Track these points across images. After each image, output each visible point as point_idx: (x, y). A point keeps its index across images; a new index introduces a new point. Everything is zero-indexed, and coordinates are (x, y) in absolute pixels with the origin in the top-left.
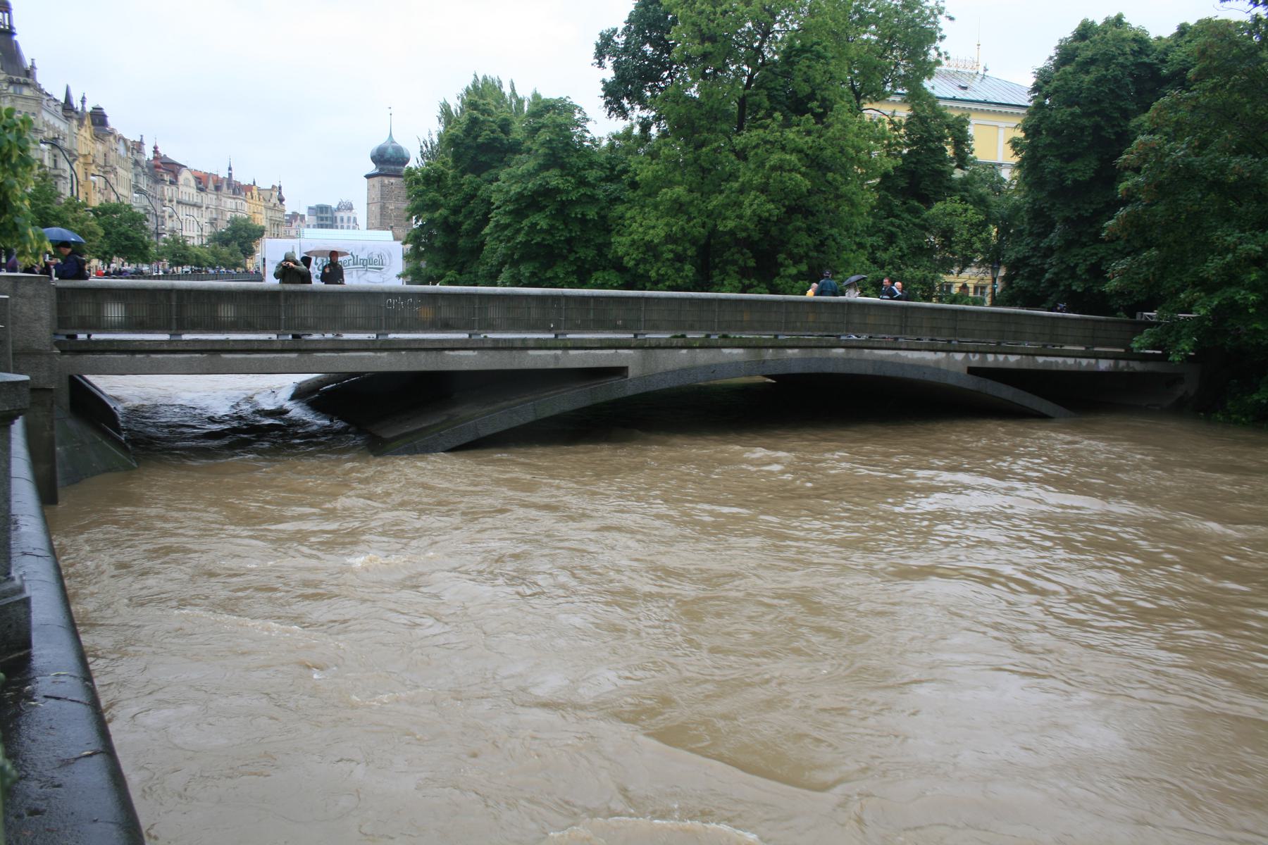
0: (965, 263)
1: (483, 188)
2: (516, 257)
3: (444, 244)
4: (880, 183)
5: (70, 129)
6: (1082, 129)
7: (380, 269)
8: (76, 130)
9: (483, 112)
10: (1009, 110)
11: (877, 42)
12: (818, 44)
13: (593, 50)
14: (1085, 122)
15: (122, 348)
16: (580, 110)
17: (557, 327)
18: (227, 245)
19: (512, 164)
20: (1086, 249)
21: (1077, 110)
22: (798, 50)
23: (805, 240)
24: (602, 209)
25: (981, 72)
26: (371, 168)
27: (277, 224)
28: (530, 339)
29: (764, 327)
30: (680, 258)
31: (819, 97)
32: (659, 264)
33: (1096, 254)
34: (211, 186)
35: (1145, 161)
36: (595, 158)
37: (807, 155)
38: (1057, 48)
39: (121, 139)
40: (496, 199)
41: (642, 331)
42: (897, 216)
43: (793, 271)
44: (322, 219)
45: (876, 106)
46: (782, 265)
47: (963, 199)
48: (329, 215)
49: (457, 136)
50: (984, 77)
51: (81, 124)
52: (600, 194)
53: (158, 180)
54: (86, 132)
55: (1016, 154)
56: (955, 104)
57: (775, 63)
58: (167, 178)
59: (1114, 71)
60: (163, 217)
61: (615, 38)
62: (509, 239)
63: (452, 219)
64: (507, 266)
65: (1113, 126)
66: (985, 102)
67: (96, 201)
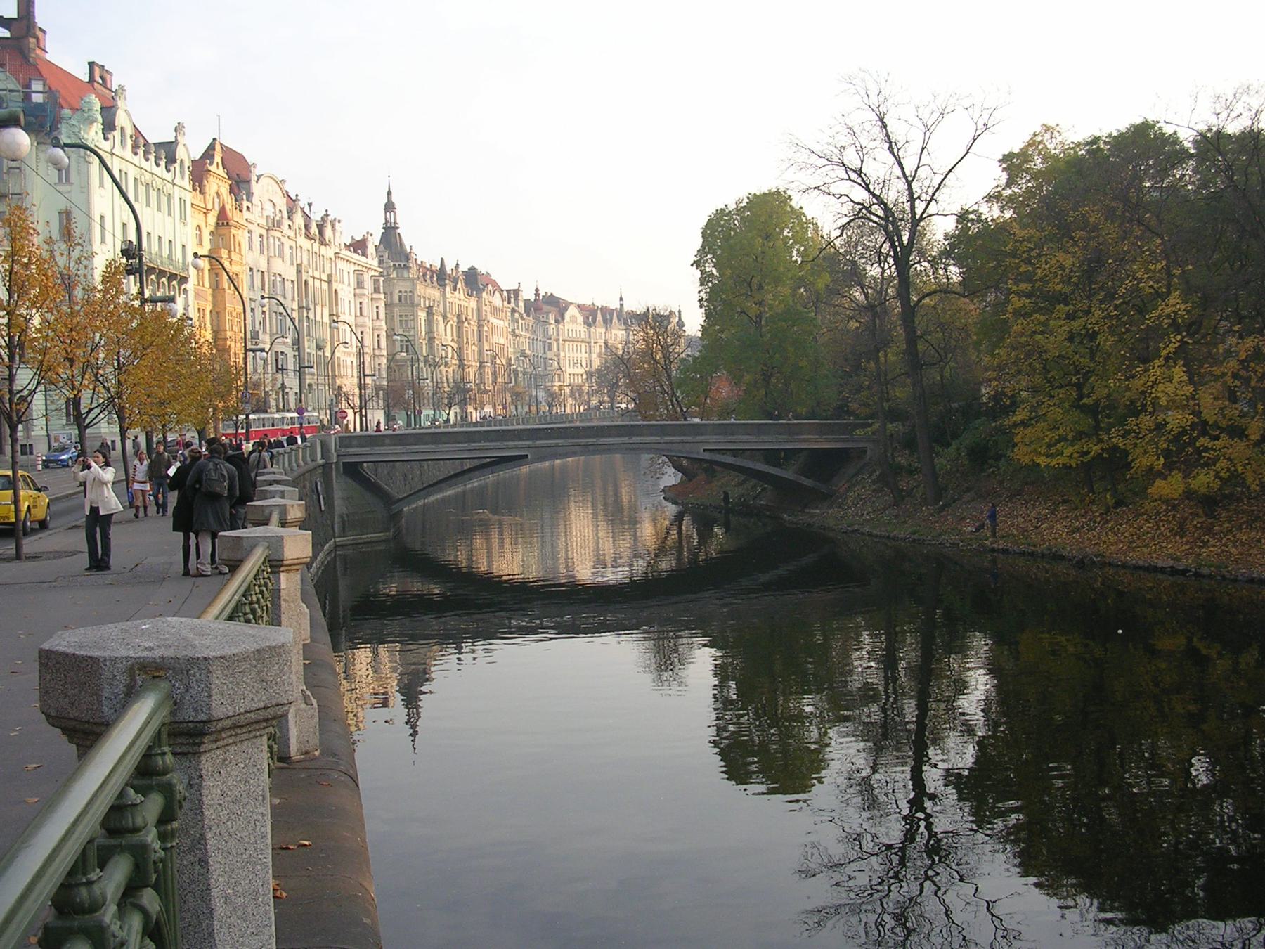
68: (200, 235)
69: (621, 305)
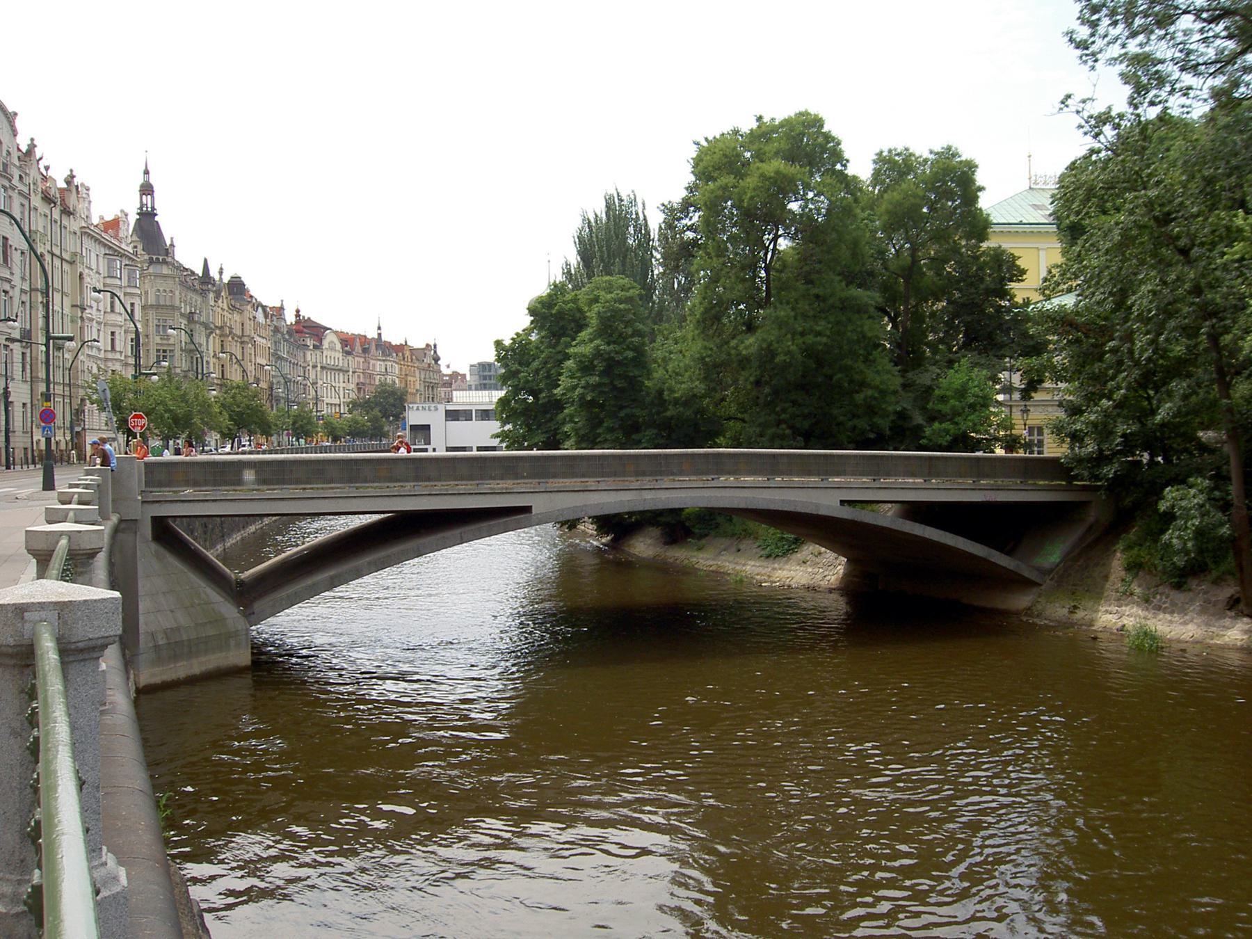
34: (358, 348)
44: (485, 378)
58: (310, 342)
68: (48, 302)
69: (380, 335)
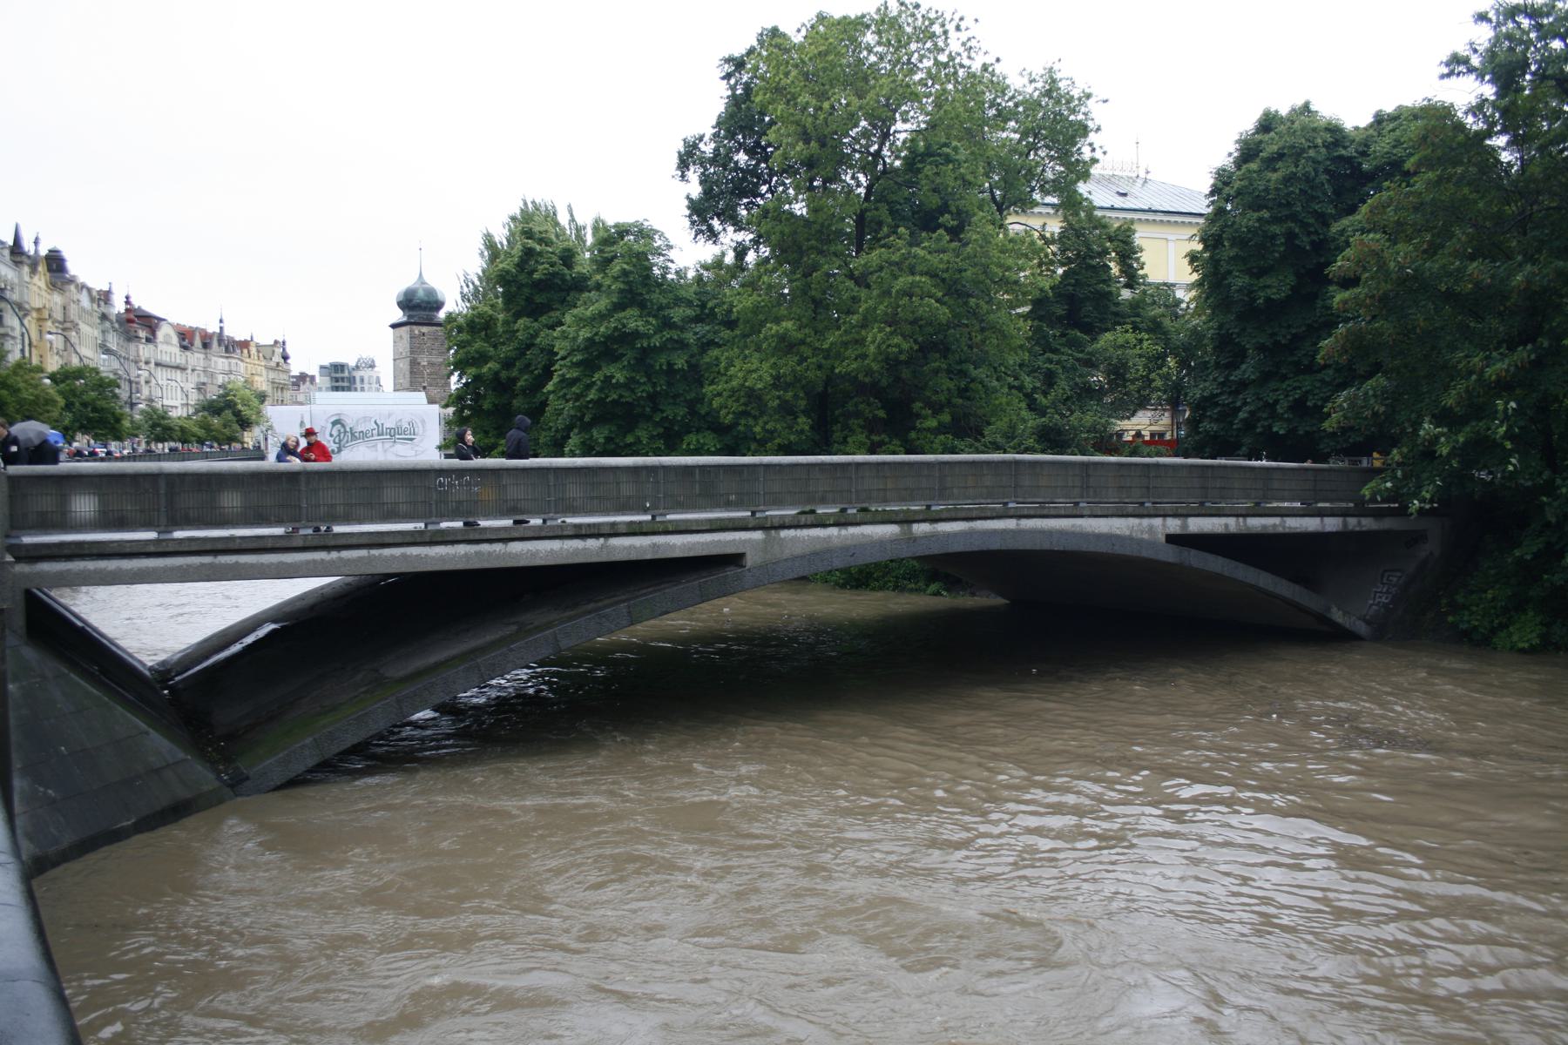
0: (1142, 404)
1: (542, 334)
2: (587, 419)
3: (495, 405)
4: (1031, 311)
5: (20, 277)
6: (1274, 237)
7: (411, 439)
8: (27, 278)
9: (541, 241)
10: (1179, 219)
11: (1020, 141)
12: (946, 145)
13: (675, 160)
14: (1276, 229)
15: (95, 551)
16: (662, 235)
17: (655, 506)
18: (219, 415)
19: (579, 303)
20: (1287, 382)
21: (1265, 214)
22: (922, 155)
23: (946, 384)
24: (692, 356)
25: (1142, 175)
26: (398, 315)
27: (282, 388)
28: (620, 523)
29: (911, 496)
30: (787, 410)
31: (953, 209)
32: (765, 418)
33: (1300, 388)
34: (198, 342)
35: (1365, 269)
36: (683, 293)
37: (943, 280)
38: (1237, 142)
39: (82, 287)
40: (561, 347)
41: (762, 508)
42: (1055, 351)
43: (932, 423)
44: (337, 380)
45: (1022, 219)
46: (918, 416)
47: (1135, 328)
48: (346, 374)
49: (508, 272)
50: (1146, 181)
51: (34, 270)
52: (690, 337)
53: (131, 338)
54: (41, 280)
55: (1195, 270)
56: (1113, 214)
57: (896, 170)
58: (142, 334)
59: (1304, 167)
60: (137, 383)
61: (702, 146)
62: (578, 397)
63: (504, 374)
64: (576, 431)
65: (1309, 233)
66: (1150, 210)
67: (53, 364)
69: (221, 328)
